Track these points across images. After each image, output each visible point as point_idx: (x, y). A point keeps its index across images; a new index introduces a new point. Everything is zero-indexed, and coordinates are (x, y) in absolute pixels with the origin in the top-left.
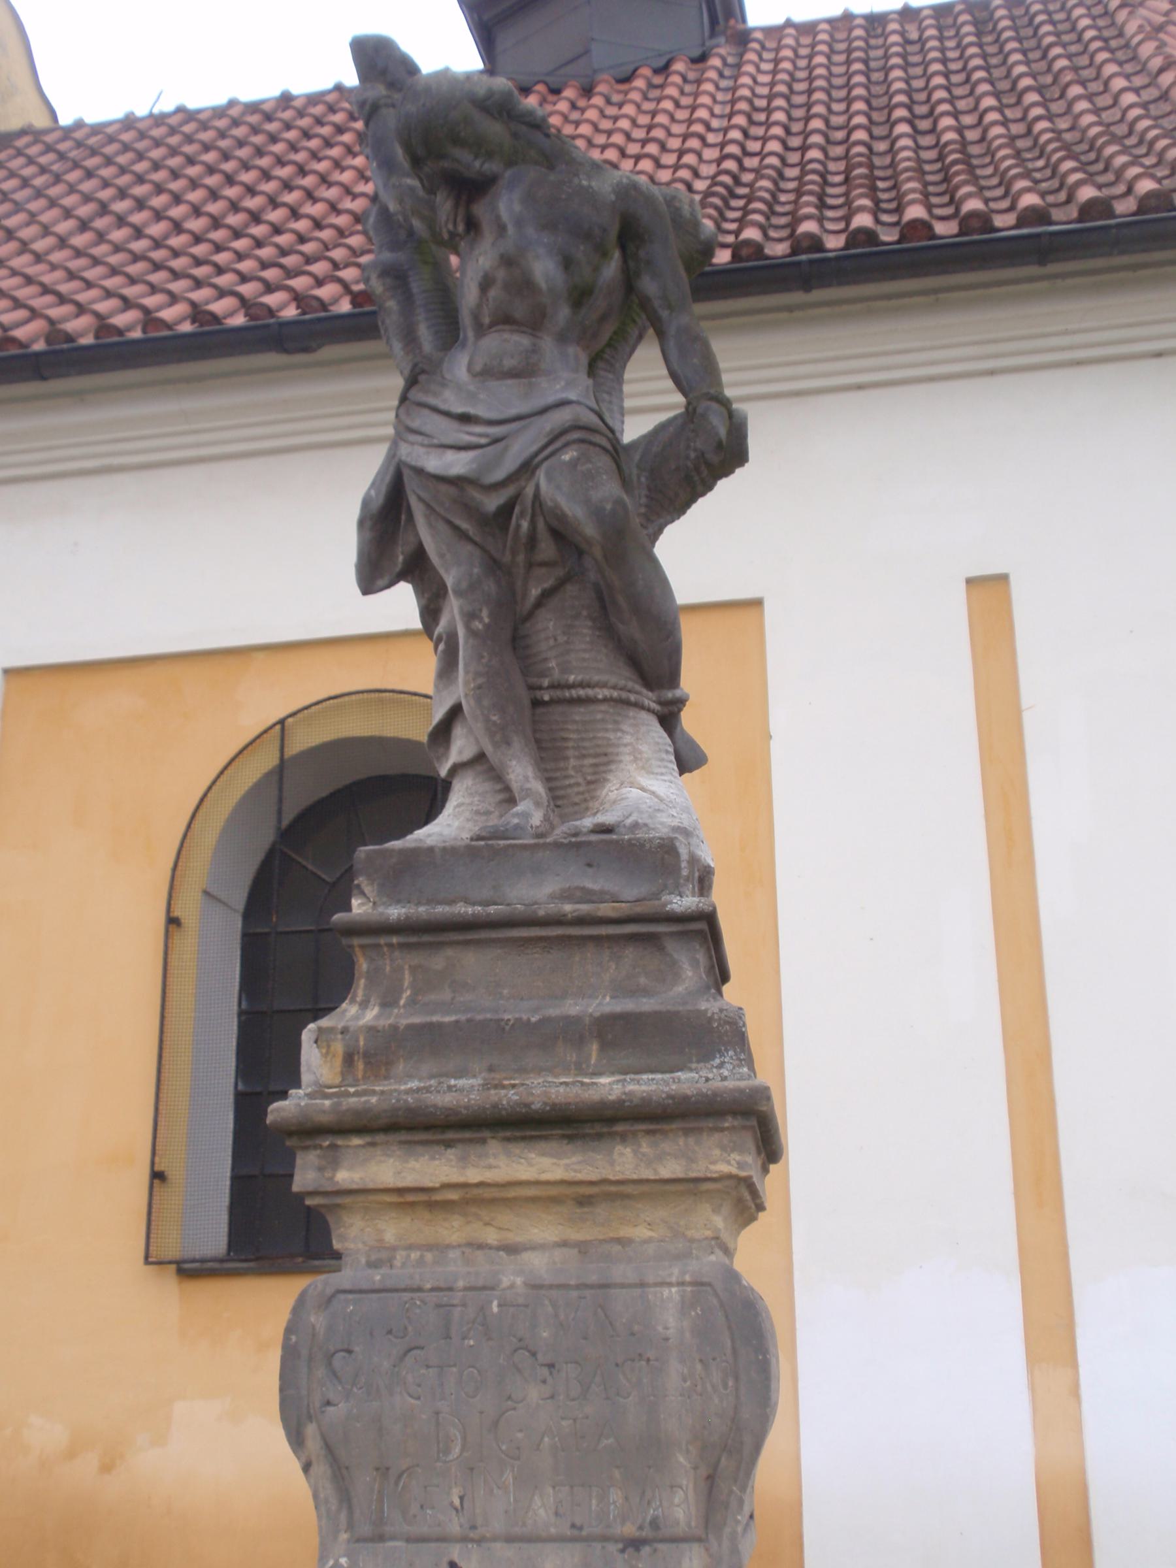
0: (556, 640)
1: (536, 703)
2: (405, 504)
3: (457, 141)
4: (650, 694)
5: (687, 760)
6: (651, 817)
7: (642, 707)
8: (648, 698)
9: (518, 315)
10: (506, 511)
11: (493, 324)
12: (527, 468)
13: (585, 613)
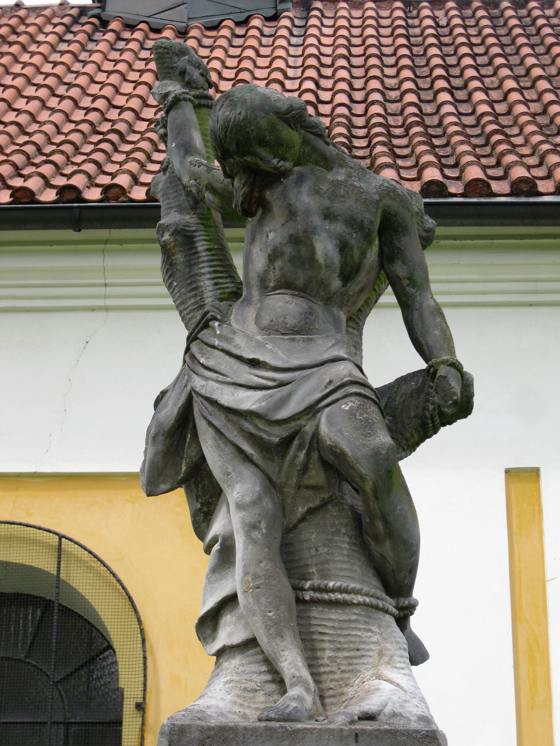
0: (317, 550)
1: (300, 601)
2: (191, 426)
3: (262, 142)
4: (392, 600)
5: (417, 655)
6: (401, 707)
7: (387, 612)
8: (390, 603)
9: (300, 282)
10: (287, 442)
11: (275, 289)
12: (312, 410)
13: (343, 530)
